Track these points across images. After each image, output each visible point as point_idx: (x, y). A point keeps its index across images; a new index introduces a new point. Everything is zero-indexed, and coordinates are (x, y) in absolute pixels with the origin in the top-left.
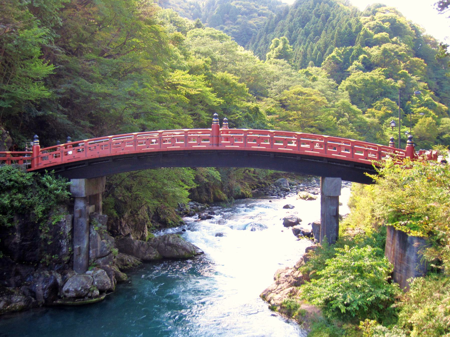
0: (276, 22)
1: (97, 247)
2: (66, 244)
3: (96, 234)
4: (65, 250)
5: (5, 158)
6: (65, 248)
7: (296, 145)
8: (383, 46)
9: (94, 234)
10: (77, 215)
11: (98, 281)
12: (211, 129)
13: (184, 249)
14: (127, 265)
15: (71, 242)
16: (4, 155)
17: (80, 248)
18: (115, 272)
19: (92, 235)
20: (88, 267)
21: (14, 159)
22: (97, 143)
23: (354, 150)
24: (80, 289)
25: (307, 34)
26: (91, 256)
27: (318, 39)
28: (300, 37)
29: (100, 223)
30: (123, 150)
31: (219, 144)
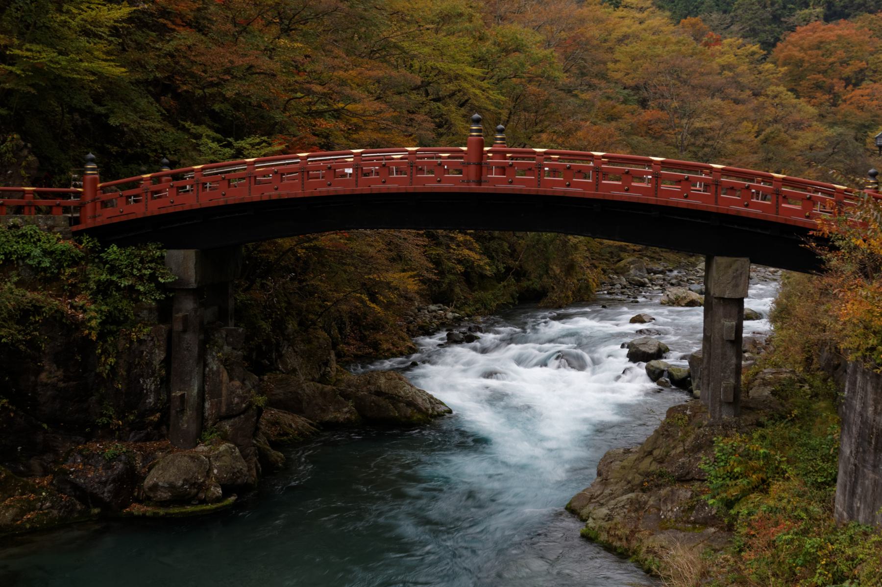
1: (220, 395)
2: (153, 387)
3: (218, 368)
4: (151, 400)
5: (22, 202)
6: (152, 396)
7: (649, 186)
9: (215, 368)
10: (178, 327)
12: (465, 149)
13: (411, 404)
14: (287, 434)
15: (165, 383)
16: (22, 193)
17: (183, 396)
18: (259, 448)
19: (211, 370)
20: (199, 438)
21: (43, 203)
22: (221, 173)
23: (781, 198)
24: (180, 483)
26: (206, 414)
29: (228, 344)
30: (276, 189)
31: (483, 178)
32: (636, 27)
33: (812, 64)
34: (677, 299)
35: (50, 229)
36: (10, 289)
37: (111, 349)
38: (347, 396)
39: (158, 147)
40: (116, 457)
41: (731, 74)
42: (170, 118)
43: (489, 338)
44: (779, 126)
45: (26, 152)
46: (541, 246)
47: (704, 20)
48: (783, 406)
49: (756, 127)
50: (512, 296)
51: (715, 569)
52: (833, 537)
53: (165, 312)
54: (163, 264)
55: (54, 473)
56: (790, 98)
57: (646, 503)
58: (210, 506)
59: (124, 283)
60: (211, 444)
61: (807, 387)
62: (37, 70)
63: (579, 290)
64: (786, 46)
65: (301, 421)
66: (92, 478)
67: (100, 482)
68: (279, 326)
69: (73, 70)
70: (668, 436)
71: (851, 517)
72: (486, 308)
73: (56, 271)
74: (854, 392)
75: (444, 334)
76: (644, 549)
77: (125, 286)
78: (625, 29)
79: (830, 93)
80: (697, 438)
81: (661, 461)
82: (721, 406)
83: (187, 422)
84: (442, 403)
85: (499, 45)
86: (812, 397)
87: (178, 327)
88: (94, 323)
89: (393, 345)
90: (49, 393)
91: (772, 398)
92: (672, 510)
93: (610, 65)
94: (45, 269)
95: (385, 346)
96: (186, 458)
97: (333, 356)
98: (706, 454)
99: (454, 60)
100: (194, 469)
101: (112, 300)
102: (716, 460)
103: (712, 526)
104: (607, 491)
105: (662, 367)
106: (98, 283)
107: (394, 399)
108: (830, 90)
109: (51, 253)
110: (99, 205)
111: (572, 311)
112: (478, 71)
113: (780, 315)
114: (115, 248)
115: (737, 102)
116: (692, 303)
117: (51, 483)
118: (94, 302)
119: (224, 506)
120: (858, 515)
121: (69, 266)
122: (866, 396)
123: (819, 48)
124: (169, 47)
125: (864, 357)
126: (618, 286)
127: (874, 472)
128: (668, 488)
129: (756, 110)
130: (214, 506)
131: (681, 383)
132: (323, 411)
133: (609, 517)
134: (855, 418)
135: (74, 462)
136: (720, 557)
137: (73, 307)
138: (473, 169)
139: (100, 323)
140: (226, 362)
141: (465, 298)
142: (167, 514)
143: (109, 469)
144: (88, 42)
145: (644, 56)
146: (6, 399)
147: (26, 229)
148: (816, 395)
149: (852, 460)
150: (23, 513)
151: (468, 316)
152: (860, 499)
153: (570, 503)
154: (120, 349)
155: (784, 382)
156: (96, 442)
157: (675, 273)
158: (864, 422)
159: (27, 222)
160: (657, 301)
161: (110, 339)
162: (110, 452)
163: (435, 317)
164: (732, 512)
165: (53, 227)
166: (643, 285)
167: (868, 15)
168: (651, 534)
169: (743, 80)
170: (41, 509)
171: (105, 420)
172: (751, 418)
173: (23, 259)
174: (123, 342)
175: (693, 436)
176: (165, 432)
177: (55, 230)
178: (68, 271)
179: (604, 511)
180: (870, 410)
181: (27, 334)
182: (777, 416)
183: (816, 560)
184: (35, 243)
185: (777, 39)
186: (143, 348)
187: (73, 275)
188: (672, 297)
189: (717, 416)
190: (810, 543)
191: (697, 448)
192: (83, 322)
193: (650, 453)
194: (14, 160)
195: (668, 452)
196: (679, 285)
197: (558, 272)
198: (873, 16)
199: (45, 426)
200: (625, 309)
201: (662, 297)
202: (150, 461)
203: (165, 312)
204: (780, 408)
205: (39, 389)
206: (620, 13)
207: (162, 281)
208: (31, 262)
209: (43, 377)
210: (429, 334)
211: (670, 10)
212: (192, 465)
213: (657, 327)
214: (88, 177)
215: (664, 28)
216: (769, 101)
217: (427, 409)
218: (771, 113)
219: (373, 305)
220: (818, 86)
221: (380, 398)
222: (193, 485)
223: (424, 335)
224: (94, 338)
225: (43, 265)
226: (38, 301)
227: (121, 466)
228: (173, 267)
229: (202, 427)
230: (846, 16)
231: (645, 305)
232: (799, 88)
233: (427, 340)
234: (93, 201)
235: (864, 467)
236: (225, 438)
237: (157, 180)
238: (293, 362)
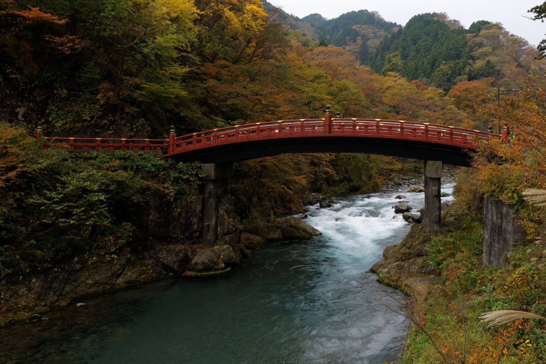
0: (391, 42)
1: (224, 225)
3: (223, 213)
4: (195, 227)
8: (487, 59)
9: (222, 213)
11: (223, 255)
13: (304, 230)
14: (252, 243)
15: (201, 220)
17: (208, 225)
18: (240, 248)
19: (220, 214)
20: (215, 243)
25: (418, 51)
27: (428, 55)
28: (413, 53)
29: (228, 203)
32: (393, 83)
33: (464, 97)
34: (414, 189)
35: (155, 156)
36: (138, 180)
37: (179, 205)
38: (278, 228)
39: (200, 125)
40: (180, 251)
41: (432, 101)
42: (204, 114)
43: (337, 206)
44: (453, 121)
45: (146, 126)
46: (358, 168)
47: (420, 81)
48: (459, 224)
49: (443, 121)
50: (346, 189)
51: (434, 291)
52: (483, 272)
53: (201, 189)
54: (201, 169)
55: (154, 258)
56: (456, 109)
57: (404, 266)
58: (219, 272)
59: (185, 177)
60: (220, 245)
61: (469, 217)
62: (152, 93)
63: (374, 187)
64: (453, 91)
65: (258, 238)
66: (170, 260)
67: (173, 262)
68: (250, 199)
69: (166, 93)
70: (412, 237)
71: (490, 264)
72: (335, 194)
73: (157, 173)
74: (488, 211)
75: (318, 205)
76: (404, 285)
77: (185, 179)
78: (389, 84)
79: (472, 108)
80: (424, 237)
81: (409, 248)
82: (433, 223)
83: (210, 236)
84: (318, 231)
85: (338, 88)
86: (471, 221)
87: (207, 196)
88: (172, 194)
89: (297, 209)
90: (153, 224)
91: (455, 221)
92: (415, 268)
93: (383, 98)
94: (153, 172)
95: (294, 209)
96: (210, 251)
97: (272, 212)
98: (428, 244)
99: (320, 93)
100: (213, 256)
101: (180, 185)
102: (432, 246)
103: (432, 274)
104: (387, 262)
105: (409, 215)
106: (174, 177)
107: (297, 228)
108: (472, 107)
109: (155, 165)
110: (175, 146)
111: (372, 195)
112: (329, 97)
113: (457, 191)
114: (181, 163)
115: (435, 111)
116: (421, 191)
117: (153, 262)
118: (173, 186)
119: (225, 272)
120: (493, 263)
121: (162, 171)
122: (493, 212)
123: (466, 91)
124: (205, 86)
125: (491, 195)
126: (390, 185)
127: (498, 244)
128: (413, 259)
129: (443, 115)
130: (221, 272)
131: (418, 221)
132: (268, 234)
133: (388, 272)
134: (489, 222)
135: (163, 254)
136: (436, 287)
137: (164, 188)
138: (327, 127)
139: (175, 194)
140: (226, 211)
141: (327, 190)
142: (201, 275)
143: (177, 256)
144: (173, 82)
145: (397, 94)
146: (135, 226)
147: (145, 156)
148: (473, 220)
149: (489, 240)
150: (140, 275)
151: (328, 197)
152: (493, 256)
153: (372, 268)
154: (183, 205)
155: (459, 215)
156: (172, 245)
157: (413, 180)
158: (493, 223)
159: (146, 153)
160: (406, 190)
161: (179, 201)
162: (178, 249)
163: (315, 198)
164: (440, 267)
165: (157, 155)
166: (400, 184)
167: (485, 78)
168: (406, 279)
169: (437, 103)
170: (148, 273)
171: (176, 235)
172: (446, 229)
173: (144, 168)
174: (184, 202)
175: (422, 237)
176: (201, 241)
177: (157, 156)
178: (162, 173)
179: (386, 270)
180: (495, 217)
181: (144, 199)
182: (457, 228)
183: (476, 281)
184: (149, 161)
185: (450, 88)
186: (192, 205)
187: (164, 174)
188: (413, 189)
189: (432, 228)
190: (473, 274)
191: (424, 241)
192: (168, 194)
193: (405, 245)
194: (142, 129)
195: (412, 244)
196: (415, 184)
197: (365, 179)
198: (487, 79)
199: (151, 238)
200: (394, 194)
201: (409, 189)
202: (194, 253)
203: (201, 189)
204: (458, 225)
205: (149, 222)
206: (386, 78)
207: (200, 176)
208: (147, 169)
209: (151, 217)
210: (312, 204)
211: (407, 77)
212: (212, 253)
213: (406, 200)
214: (172, 135)
215: (405, 84)
216: (448, 111)
217: (311, 233)
218: (449, 116)
219: (288, 190)
220: (467, 106)
221: (292, 228)
222: (212, 262)
223: (310, 205)
224: (172, 201)
225: (152, 170)
226: (149, 185)
227: (182, 255)
228: (205, 171)
229: (216, 238)
230: (477, 79)
231: (401, 192)
232: (460, 107)
233: (311, 207)
234: (173, 144)
235: (494, 242)
236: (226, 243)
237: (199, 135)
238: (255, 214)
